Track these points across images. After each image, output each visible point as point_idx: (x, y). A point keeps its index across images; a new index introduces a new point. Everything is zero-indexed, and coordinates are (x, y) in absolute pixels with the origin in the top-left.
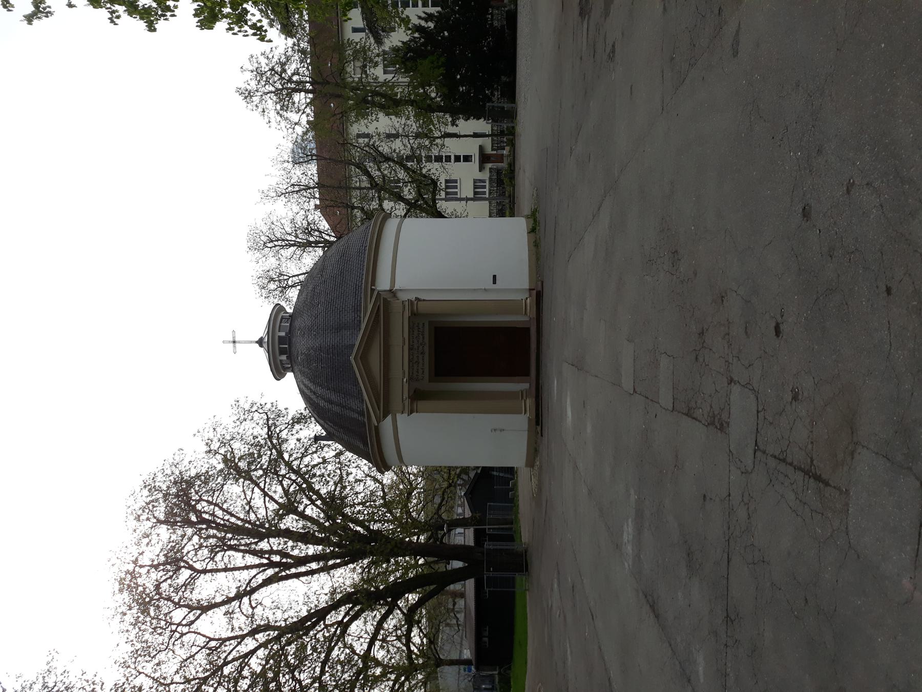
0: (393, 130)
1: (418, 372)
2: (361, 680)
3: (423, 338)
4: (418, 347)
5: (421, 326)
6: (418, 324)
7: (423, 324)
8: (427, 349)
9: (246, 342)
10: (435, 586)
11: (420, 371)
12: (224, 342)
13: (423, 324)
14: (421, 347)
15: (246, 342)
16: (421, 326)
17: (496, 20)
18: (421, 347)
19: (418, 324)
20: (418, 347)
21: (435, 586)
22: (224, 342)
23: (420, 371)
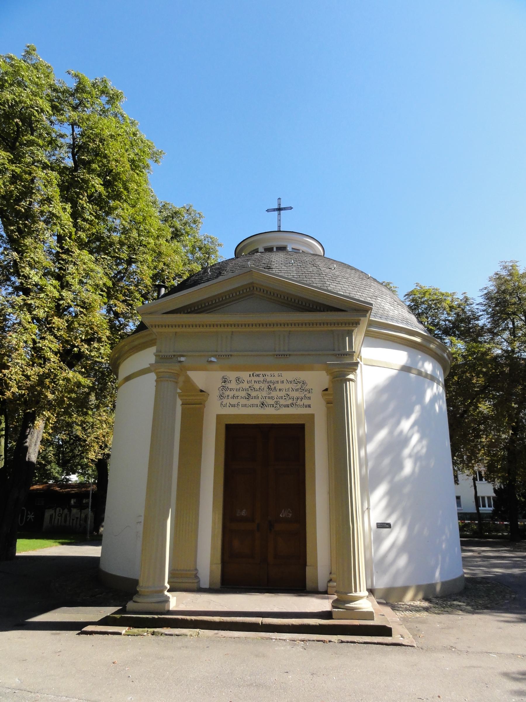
0: (54, 237)
1: (234, 397)
2: (13, 424)
3: (288, 406)
4: (272, 398)
5: (306, 402)
6: (309, 398)
7: (309, 406)
8: (269, 411)
9: (279, 220)
10: (121, 607)
11: (234, 402)
12: (291, 208)
13: (309, 406)
14: (271, 402)
15: (279, 220)
16: (306, 402)
17: (385, 397)
18: (271, 402)
19: (309, 398)
20: (272, 398)
21: (121, 607)
22: (291, 208)
23: (234, 402)
